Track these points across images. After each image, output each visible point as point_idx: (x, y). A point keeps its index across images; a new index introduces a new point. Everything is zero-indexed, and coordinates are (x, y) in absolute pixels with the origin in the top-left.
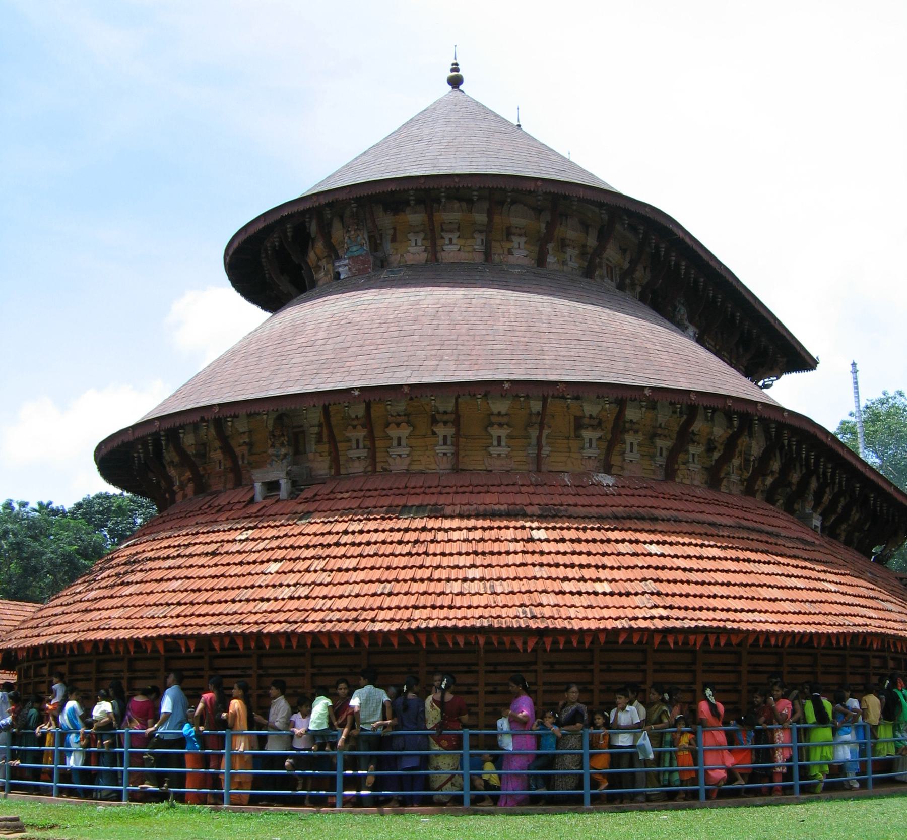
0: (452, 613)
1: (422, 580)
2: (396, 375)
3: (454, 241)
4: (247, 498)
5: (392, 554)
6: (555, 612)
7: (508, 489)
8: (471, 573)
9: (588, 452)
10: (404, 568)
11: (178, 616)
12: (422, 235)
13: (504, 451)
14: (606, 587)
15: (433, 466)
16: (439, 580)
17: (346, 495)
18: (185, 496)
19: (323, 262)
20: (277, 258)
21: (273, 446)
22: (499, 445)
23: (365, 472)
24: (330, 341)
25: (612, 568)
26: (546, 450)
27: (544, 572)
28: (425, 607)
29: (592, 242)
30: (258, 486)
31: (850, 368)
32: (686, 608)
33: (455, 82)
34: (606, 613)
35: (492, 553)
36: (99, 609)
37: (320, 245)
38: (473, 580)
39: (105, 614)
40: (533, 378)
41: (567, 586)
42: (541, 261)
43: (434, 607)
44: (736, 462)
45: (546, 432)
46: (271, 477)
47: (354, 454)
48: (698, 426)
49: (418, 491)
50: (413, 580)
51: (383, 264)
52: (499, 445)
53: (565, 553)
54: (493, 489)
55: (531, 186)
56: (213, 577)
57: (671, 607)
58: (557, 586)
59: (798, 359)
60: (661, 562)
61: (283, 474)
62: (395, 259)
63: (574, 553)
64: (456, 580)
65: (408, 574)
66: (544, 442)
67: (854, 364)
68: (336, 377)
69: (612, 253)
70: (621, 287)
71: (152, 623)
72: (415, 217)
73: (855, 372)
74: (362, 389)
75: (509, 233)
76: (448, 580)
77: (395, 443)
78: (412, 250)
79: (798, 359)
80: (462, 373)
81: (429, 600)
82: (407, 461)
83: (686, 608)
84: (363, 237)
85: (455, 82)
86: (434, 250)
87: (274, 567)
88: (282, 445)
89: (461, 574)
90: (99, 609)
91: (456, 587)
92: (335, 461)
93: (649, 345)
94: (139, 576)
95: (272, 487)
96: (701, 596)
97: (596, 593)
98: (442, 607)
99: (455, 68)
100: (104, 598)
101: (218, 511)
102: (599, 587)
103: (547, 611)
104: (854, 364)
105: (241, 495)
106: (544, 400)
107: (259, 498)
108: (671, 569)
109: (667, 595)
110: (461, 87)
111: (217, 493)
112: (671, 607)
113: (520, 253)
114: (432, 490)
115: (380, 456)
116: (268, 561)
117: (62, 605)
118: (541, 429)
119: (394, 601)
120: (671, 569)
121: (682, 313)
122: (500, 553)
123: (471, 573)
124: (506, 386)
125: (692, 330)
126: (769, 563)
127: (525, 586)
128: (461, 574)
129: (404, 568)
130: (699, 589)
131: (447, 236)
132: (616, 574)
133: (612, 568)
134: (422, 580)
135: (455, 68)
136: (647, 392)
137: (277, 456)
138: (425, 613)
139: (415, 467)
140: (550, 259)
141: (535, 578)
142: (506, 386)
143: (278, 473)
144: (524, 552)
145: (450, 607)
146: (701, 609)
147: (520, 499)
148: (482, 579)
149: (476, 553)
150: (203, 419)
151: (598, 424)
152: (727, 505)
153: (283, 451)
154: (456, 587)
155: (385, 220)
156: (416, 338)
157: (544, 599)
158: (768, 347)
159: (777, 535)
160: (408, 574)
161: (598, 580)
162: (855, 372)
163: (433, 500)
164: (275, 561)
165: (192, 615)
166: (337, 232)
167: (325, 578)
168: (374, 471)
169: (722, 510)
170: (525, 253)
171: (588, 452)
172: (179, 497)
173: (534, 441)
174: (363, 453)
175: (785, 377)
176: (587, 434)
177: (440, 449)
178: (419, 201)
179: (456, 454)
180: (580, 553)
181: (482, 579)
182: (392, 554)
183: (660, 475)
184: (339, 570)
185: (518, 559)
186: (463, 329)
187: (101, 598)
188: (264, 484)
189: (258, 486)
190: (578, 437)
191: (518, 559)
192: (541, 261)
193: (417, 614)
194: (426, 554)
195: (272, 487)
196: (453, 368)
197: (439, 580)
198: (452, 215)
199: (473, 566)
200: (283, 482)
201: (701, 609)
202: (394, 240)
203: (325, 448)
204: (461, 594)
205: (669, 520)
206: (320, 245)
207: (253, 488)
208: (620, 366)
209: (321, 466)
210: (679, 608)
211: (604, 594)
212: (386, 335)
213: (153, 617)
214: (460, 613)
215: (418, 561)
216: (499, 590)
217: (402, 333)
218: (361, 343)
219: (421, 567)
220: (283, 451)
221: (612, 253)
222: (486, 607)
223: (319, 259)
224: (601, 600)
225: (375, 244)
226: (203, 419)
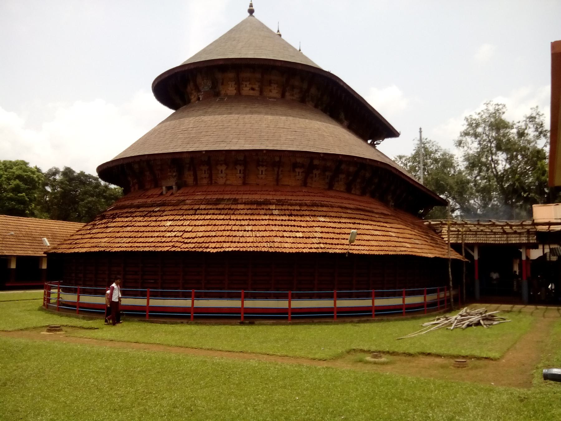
0: (239, 245)
1: (228, 230)
2: (221, 145)
3: (248, 86)
4: (159, 193)
5: (217, 219)
6: (279, 245)
7: (264, 193)
8: (247, 228)
9: (298, 177)
10: (221, 225)
11: (129, 242)
12: (234, 83)
13: (263, 176)
14: (300, 235)
15: (235, 182)
16: (235, 231)
17: (199, 193)
18: (135, 189)
19: (193, 92)
20: (175, 88)
21: (170, 172)
22: (262, 174)
23: (208, 184)
24: (195, 129)
25: (304, 227)
26: (281, 176)
27: (277, 228)
28: (228, 242)
29: (305, 86)
30: (164, 188)
31: (419, 130)
32: (332, 244)
33: (251, 12)
34: (299, 246)
35: (256, 220)
36: (96, 238)
37: (192, 84)
38: (248, 231)
39: (99, 240)
40: (275, 149)
41: (285, 234)
42: (283, 96)
43: (232, 242)
44: (359, 180)
45: (281, 169)
46: (170, 184)
47: (204, 176)
48: (343, 167)
49: (228, 192)
50: (224, 230)
51: (217, 94)
52: (262, 174)
53: (285, 220)
54: (259, 193)
55: (279, 64)
56: (144, 226)
57: (326, 243)
58: (281, 234)
59: (391, 133)
60: (324, 224)
61: (174, 184)
62: (223, 92)
63: (289, 220)
64: (241, 231)
65: (223, 228)
66: (280, 173)
67: (420, 129)
68: (196, 145)
69: (313, 91)
70: (316, 106)
71: (119, 245)
72: (231, 75)
73: (421, 132)
74: (206, 151)
75: (270, 83)
76: (238, 231)
77: (220, 172)
78: (230, 89)
79: (391, 133)
80: (247, 145)
81: (230, 239)
82: (225, 179)
83: (332, 244)
84: (209, 84)
85: (251, 12)
86: (239, 89)
87: (169, 223)
88: (174, 172)
89: (243, 228)
90: (96, 238)
91: (241, 234)
92: (196, 179)
93: (325, 134)
94: (112, 225)
95: (169, 188)
96: (338, 239)
97: (296, 237)
98: (235, 242)
99: (251, 6)
100: (99, 233)
101: (147, 198)
102: (298, 235)
103: (276, 245)
104: (420, 129)
105: (157, 191)
106: (280, 157)
107: (164, 193)
108: (327, 227)
109: (325, 238)
110: (253, 14)
111: (147, 190)
112: (326, 243)
113: (275, 92)
114: (234, 192)
115: (214, 177)
116: (167, 220)
117: (81, 235)
118: (279, 168)
119: (215, 239)
120: (327, 227)
121: (342, 116)
122: (259, 220)
123: (247, 228)
124: (265, 152)
125: (346, 123)
126: (368, 224)
127: (267, 234)
128: (243, 228)
129: (221, 225)
130: (338, 236)
131: (245, 83)
132: (305, 230)
133: (304, 227)
134: (228, 230)
135: (251, 6)
136: (322, 155)
137: (172, 176)
138: (228, 245)
139: (228, 182)
140: (287, 94)
141: (272, 231)
142: (265, 152)
143: (172, 182)
144: (269, 219)
145: (238, 242)
146: (338, 244)
147: (269, 197)
148: (252, 231)
149: (250, 220)
150: (141, 160)
151: (302, 166)
152: (353, 200)
153: (174, 174)
154: (241, 234)
155: (219, 76)
156: (229, 129)
157: (276, 239)
158: (373, 126)
159: (373, 212)
160: (223, 228)
161: (298, 232)
162: (421, 132)
163: (234, 197)
164: (170, 220)
165: (135, 242)
166: (199, 80)
167: (189, 229)
168: (211, 183)
169: (351, 202)
170: (277, 91)
171: (298, 177)
172: (132, 189)
173: (276, 172)
174: (207, 175)
175: (386, 140)
176: (297, 170)
177: (238, 175)
178: (499, 359)
179: (244, 178)
180: (291, 220)
181: (252, 231)
182: (217, 219)
183: (327, 187)
184: (195, 226)
185: (266, 222)
186: (248, 126)
187: (98, 233)
188: (166, 187)
189: (164, 188)
190: (294, 171)
191: (266, 222)
192: (283, 96)
193: (225, 245)
194: (230, 219)
195: (169, 188)
196: (243, 143)
197: (235, 231)
198: (246, 75)
199: (248, 225)
200: (174, 187)
201: (338, 244)
202: (222, 84)
203: (192, 173)
204: (243, 236)
205: (328, 206)
206: (192, 84)
207: (162, 188)
208: (311, 143)
209: (190, 180)
210: (329, 244)
211: (300, 237)
212: (217, 127)
213: (119, 243)
214: (241, 245)
215: (226, 222)
216: (258, 235)
217: (224, 127)
218: (207, 130)
219: (227, 225)
220: (174, 174)
221: (313, 91)
222: (252, 242)
223: (192, 90)
224: (298, 240)
225: (214, 86)
226: (141, 160)
